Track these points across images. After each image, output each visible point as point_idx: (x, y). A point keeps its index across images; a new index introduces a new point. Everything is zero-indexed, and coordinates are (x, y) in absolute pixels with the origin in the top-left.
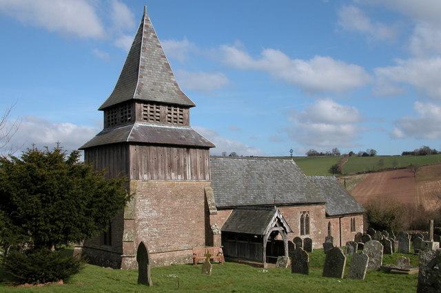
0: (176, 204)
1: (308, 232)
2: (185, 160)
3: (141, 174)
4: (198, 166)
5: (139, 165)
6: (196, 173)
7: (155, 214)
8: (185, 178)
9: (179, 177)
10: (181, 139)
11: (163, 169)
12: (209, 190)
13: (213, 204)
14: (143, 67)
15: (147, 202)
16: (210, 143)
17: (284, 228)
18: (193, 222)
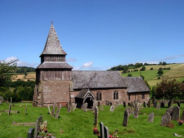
0: (58, 88)
1: (117, 98)
2: (61, 73)
3: (45, 78)
4: (13, 73)
5: (44, 75)
6: (66, 77)
7: (50, 91)
8: (62, 79)
9: (59, 79)
10: (60, 66)
11: (53, 76)
12: (71, 83)
13: (72, 88)
14: (49, 43)
15: (47, 87)
16: (72, 67)
17: (93, 96)
18: (65, 94)
